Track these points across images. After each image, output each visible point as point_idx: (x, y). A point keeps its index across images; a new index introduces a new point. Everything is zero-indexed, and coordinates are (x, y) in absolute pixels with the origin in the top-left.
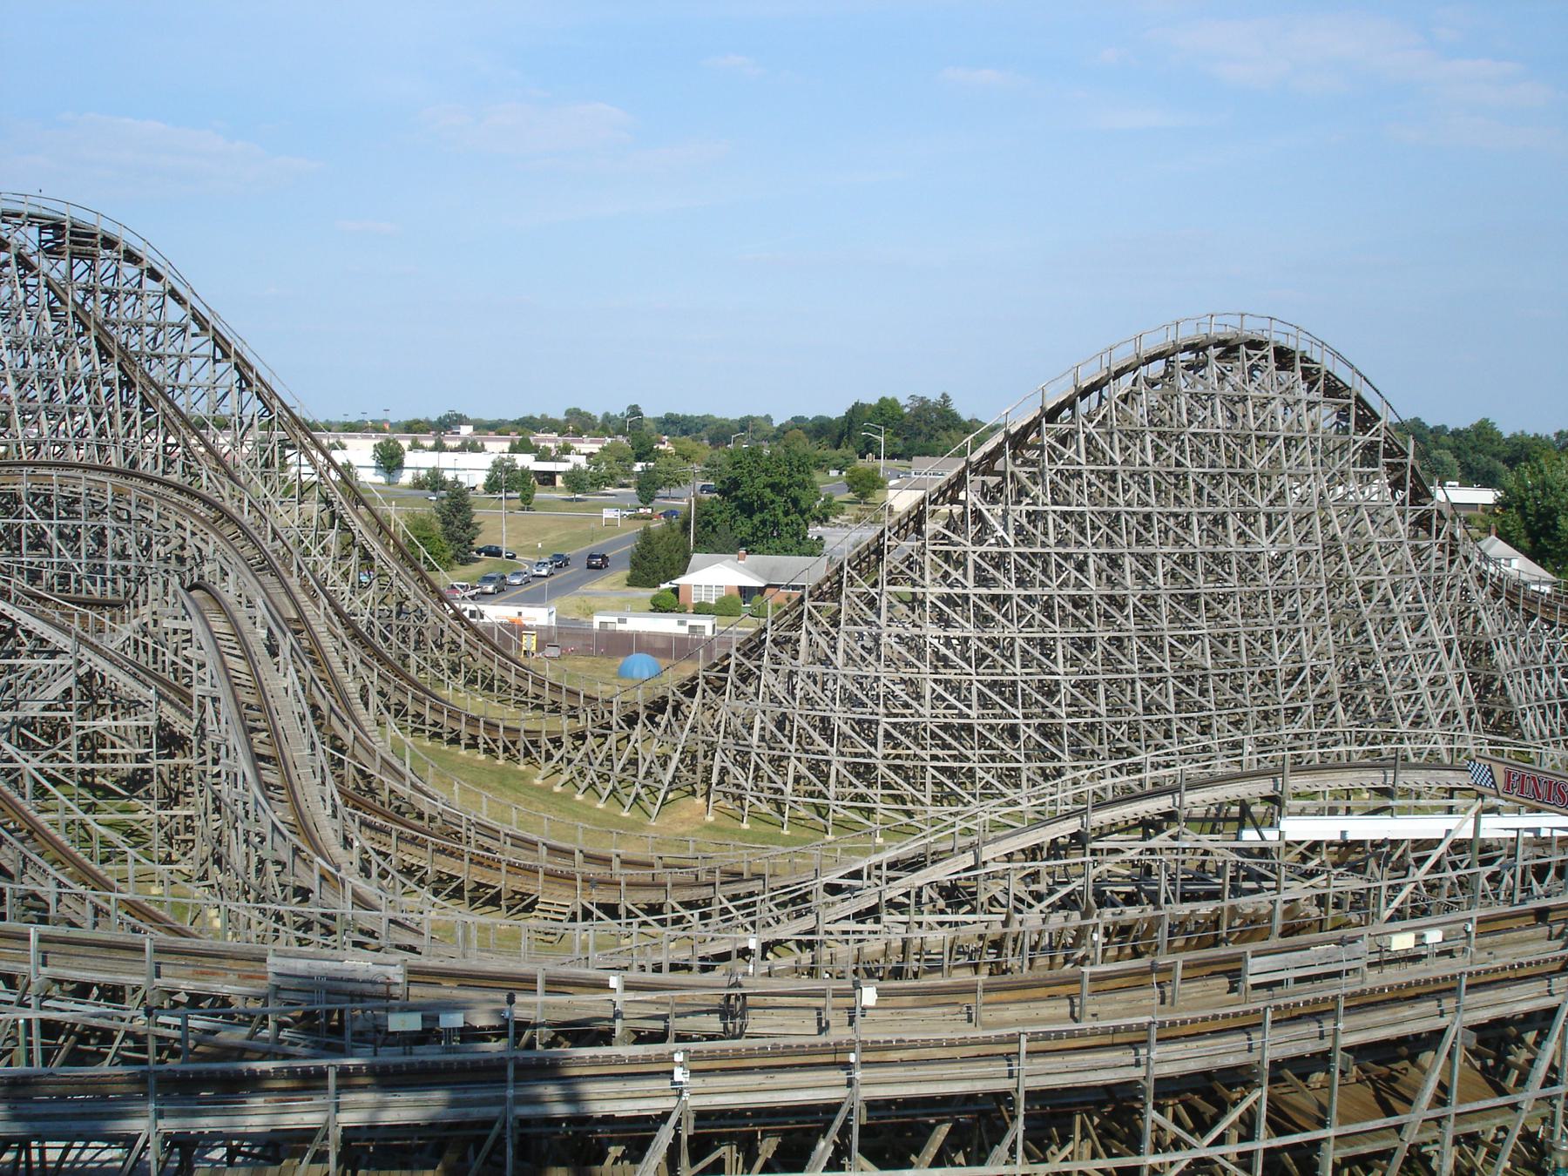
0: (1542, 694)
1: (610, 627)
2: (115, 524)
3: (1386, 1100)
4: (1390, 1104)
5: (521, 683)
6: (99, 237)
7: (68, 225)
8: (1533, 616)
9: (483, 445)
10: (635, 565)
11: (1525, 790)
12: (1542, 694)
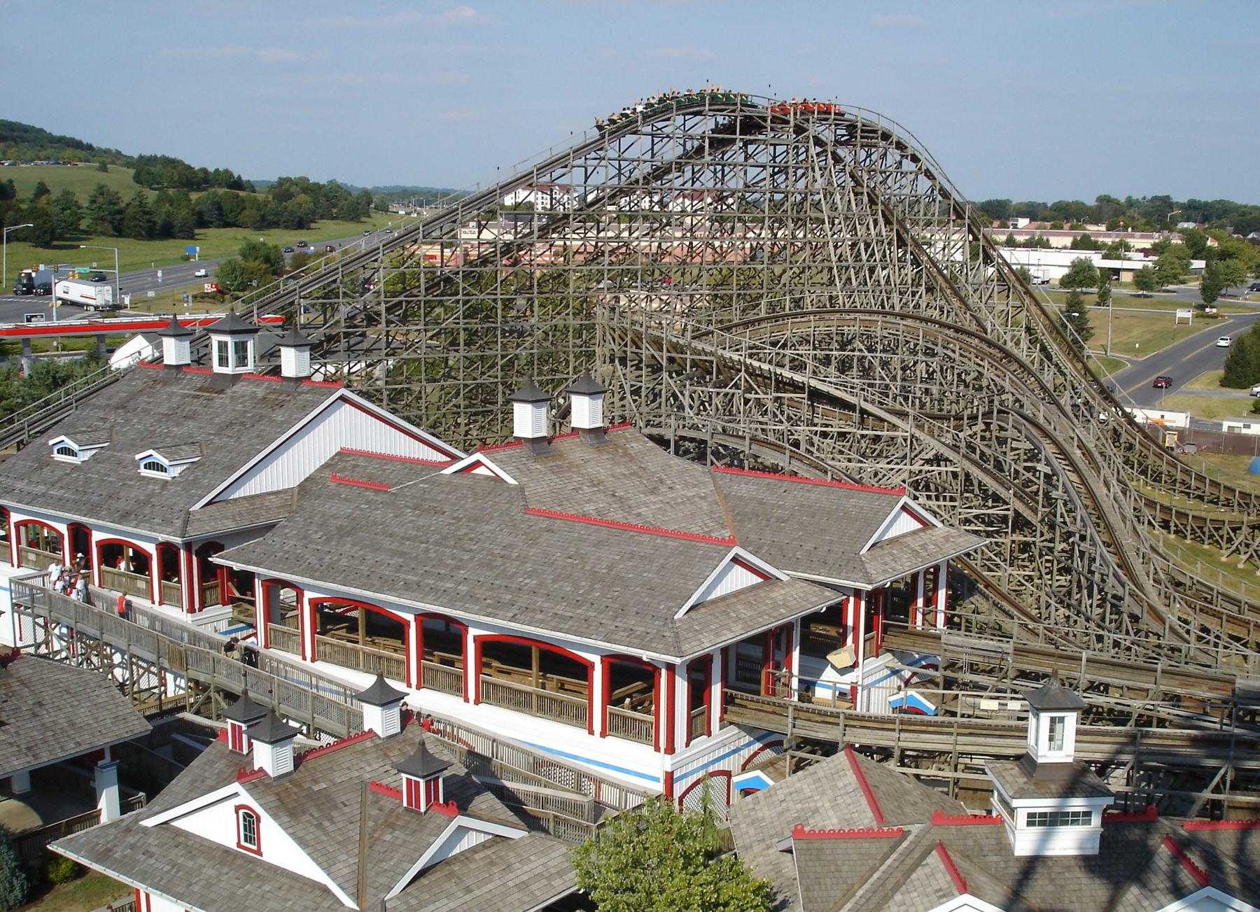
1: (1236, 431)
2: (924, 358)
5: (1187, 479)
6: (880, 132)
7: (859, 125)
9: (1048, 240)
10: (1229, 368)
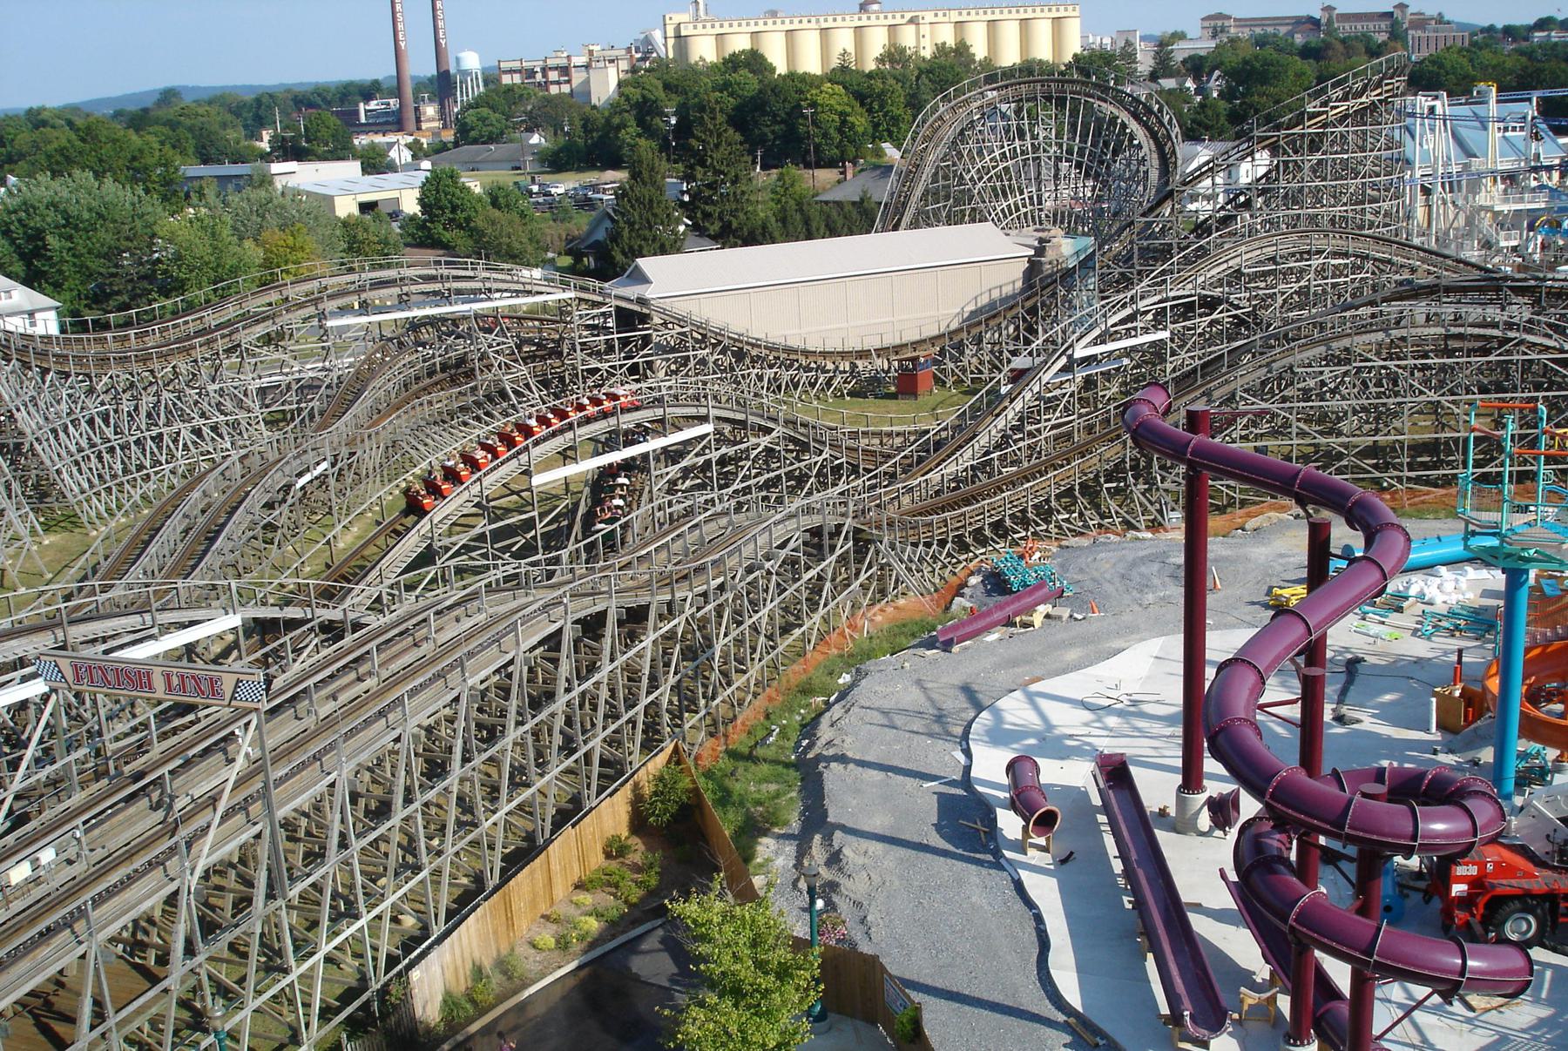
0: (73, 449)
3: (47, 1024)
4: (52, 1029)
8: (47, 371)
11: (95, 680)
12: (73, 449)
